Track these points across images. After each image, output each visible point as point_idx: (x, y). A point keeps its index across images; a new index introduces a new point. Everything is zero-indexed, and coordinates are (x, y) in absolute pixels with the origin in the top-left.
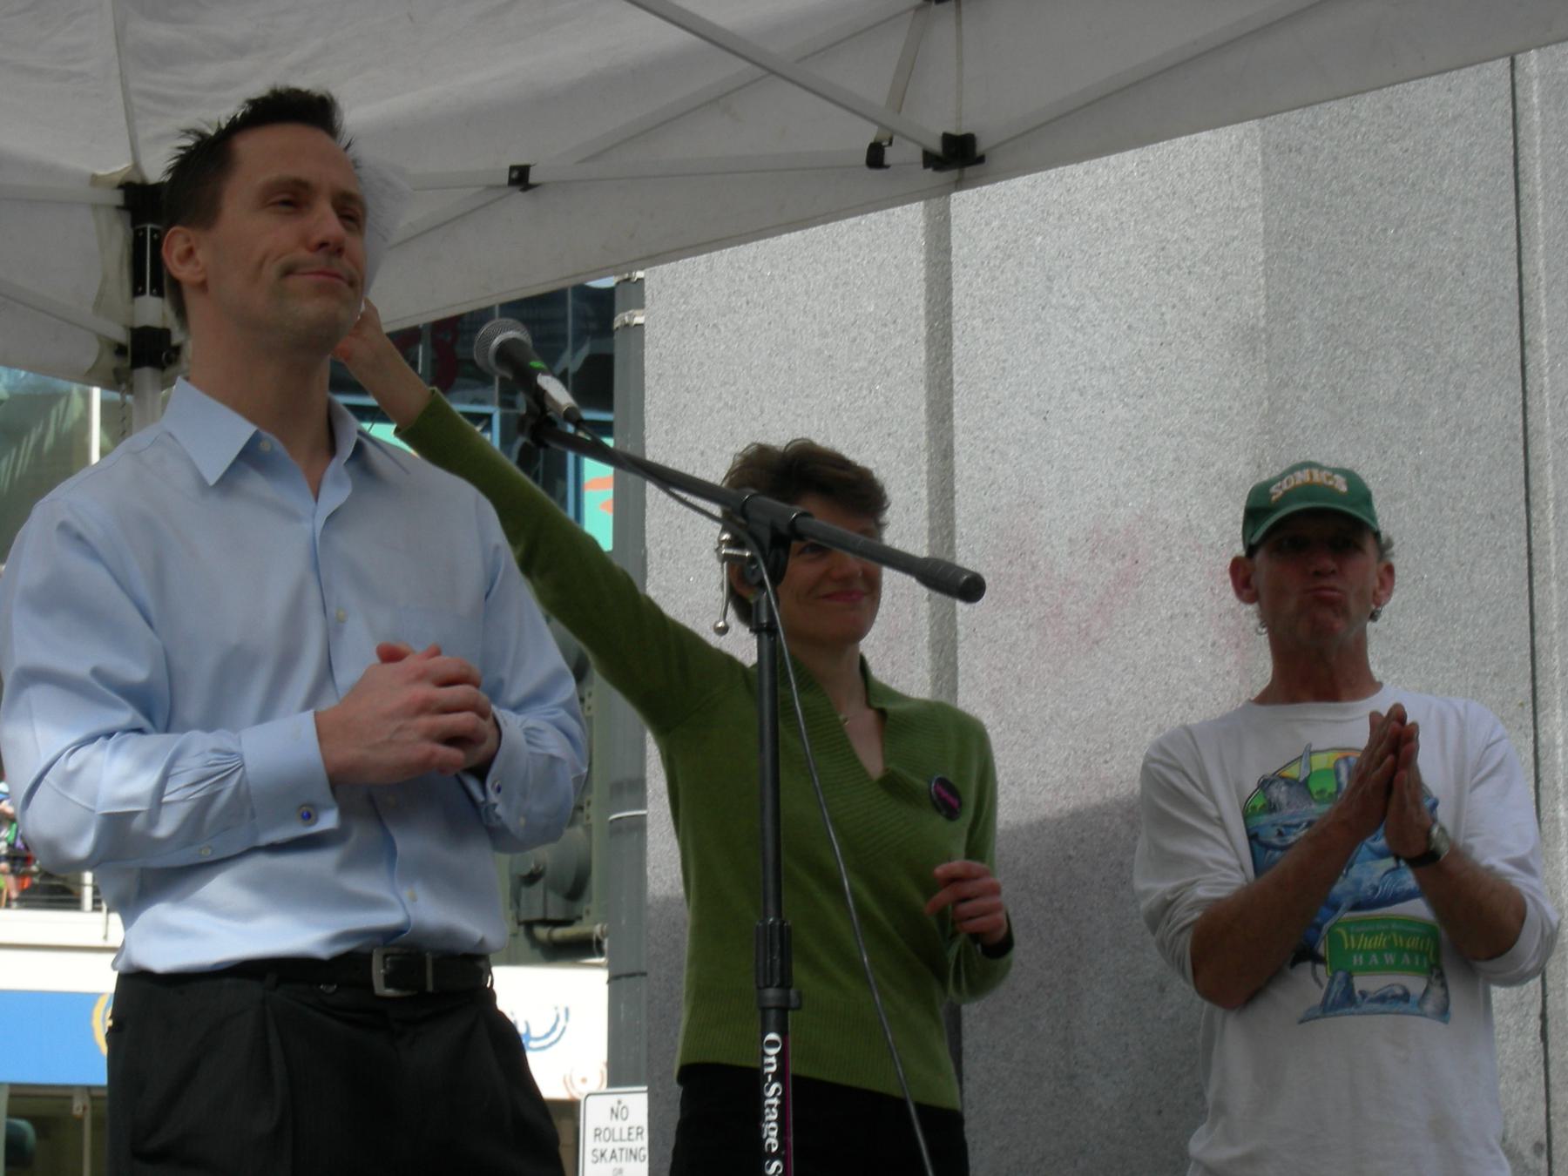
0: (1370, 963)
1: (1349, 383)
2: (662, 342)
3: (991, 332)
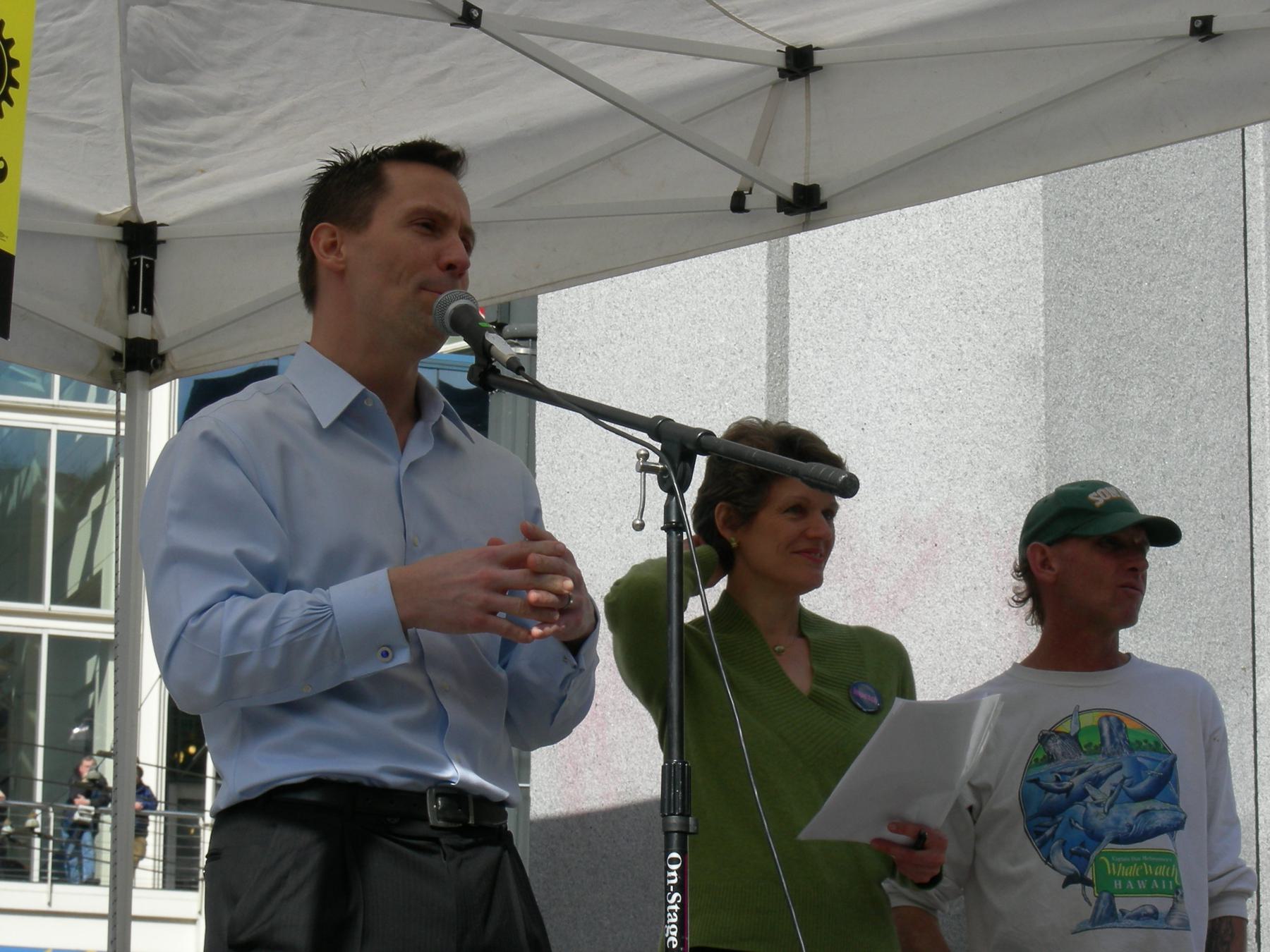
1: (1110, 404)
2: (551, 367)
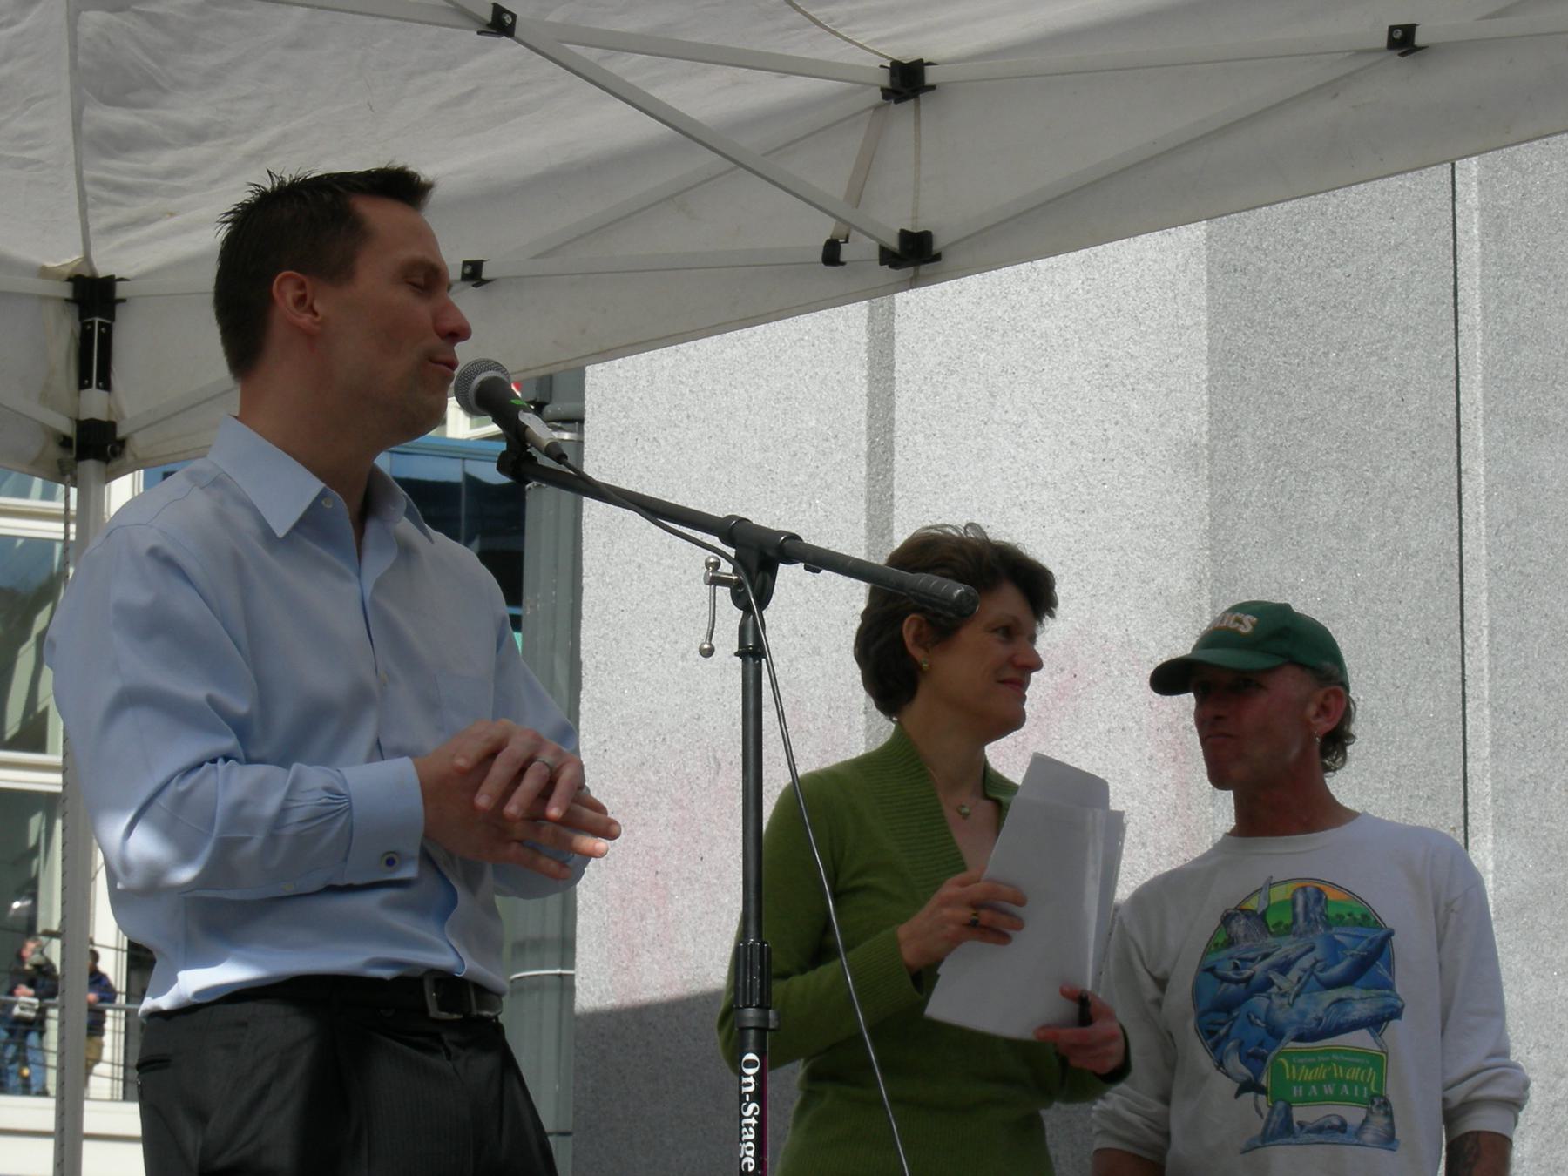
0: (1310, 1094)
1: (1290, 503)
2: (602, 455)
3: (933, 447)
